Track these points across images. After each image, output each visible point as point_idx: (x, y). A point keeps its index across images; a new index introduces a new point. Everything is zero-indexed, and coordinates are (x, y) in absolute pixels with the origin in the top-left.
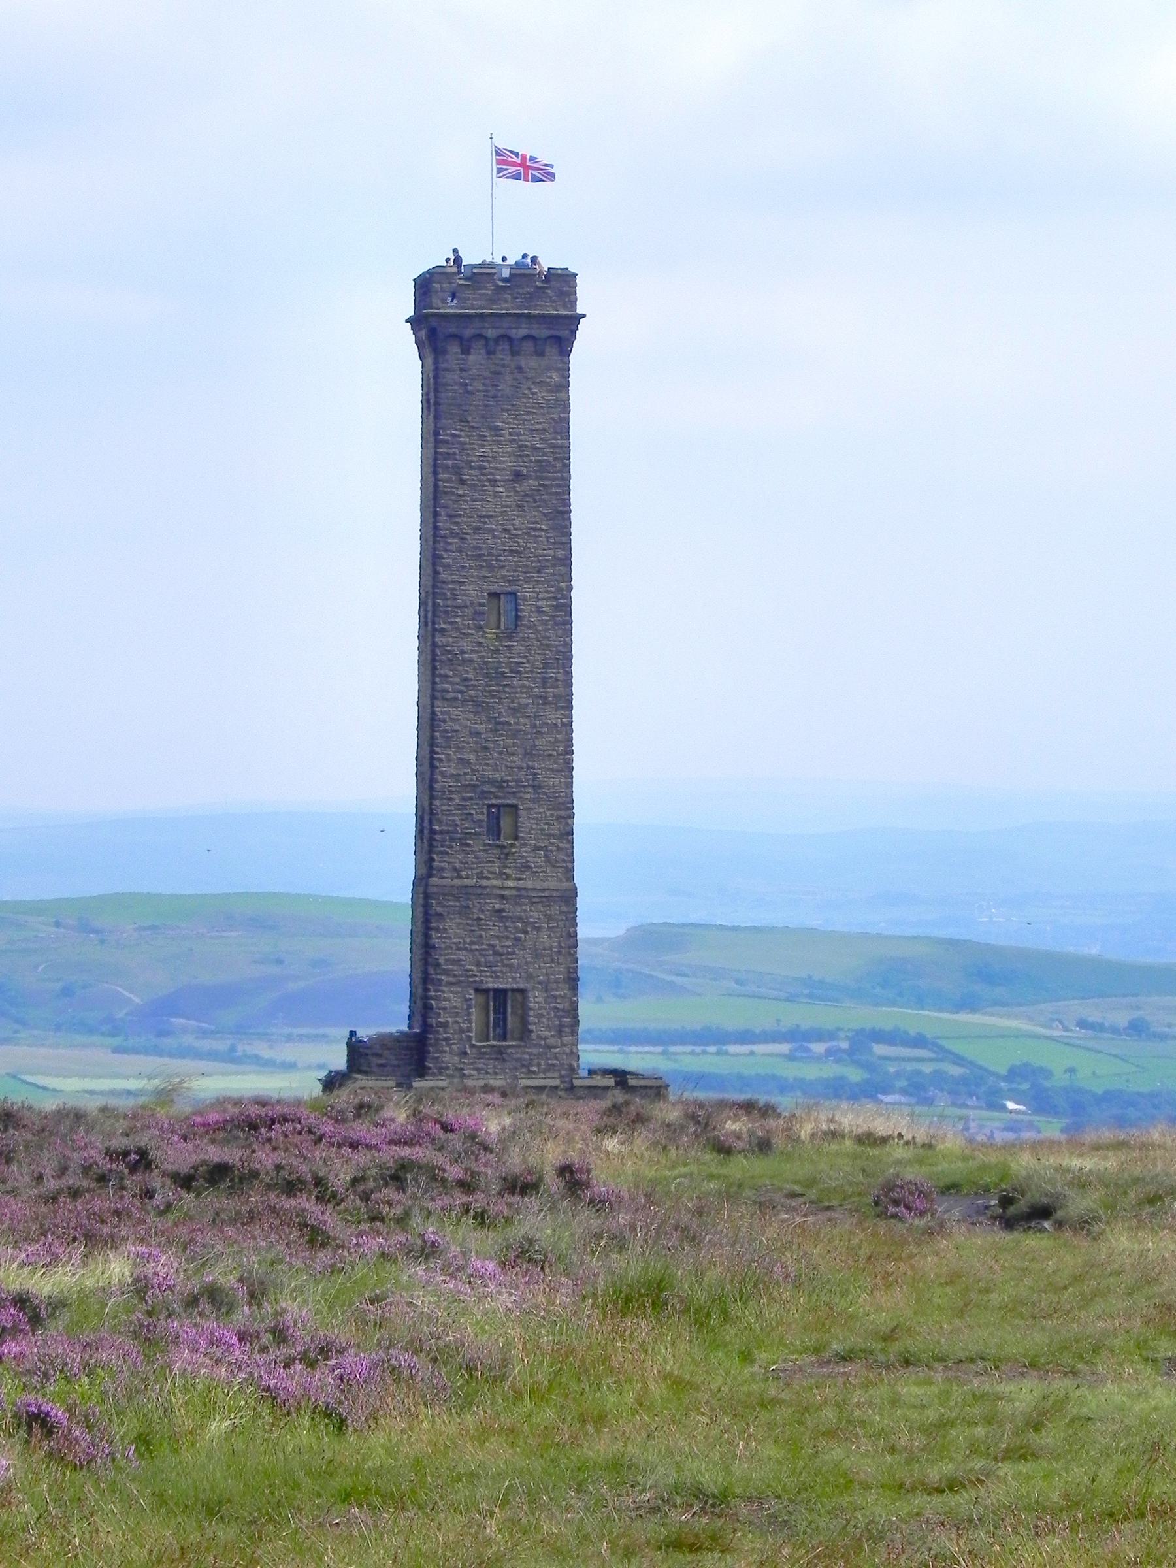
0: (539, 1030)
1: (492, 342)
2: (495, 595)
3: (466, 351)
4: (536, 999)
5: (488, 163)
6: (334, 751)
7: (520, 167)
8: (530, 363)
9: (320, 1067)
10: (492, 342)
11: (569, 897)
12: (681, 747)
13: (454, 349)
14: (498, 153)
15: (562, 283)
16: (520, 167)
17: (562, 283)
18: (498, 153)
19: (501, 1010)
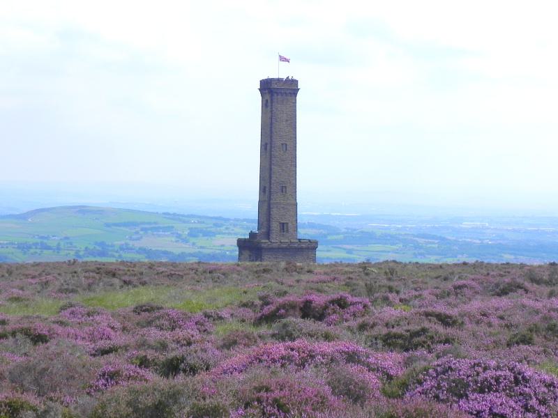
0: (291, 230)
1: (278, 96)
2: (282, 144)
3: (277, 95)
4: (290, 224)
5: (278, 58)
6: (236, 188)
7: (283, 59)
8: (289, 98)
9: (248, 228)
10: (278, 96)
11: (296, 205)
12: (320, 191)
13: (275, 95)
14: (280, 56)
15: (316, 243)
16: (283, 59)
17: (316, 243)
18: (280, 56)
19: (283, 226)
